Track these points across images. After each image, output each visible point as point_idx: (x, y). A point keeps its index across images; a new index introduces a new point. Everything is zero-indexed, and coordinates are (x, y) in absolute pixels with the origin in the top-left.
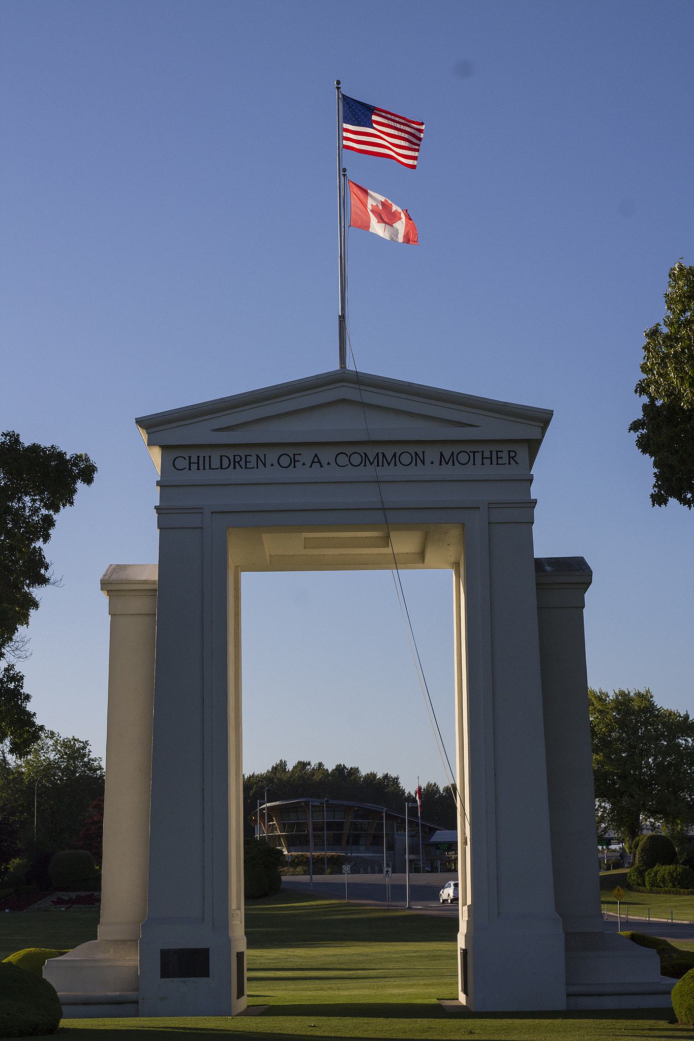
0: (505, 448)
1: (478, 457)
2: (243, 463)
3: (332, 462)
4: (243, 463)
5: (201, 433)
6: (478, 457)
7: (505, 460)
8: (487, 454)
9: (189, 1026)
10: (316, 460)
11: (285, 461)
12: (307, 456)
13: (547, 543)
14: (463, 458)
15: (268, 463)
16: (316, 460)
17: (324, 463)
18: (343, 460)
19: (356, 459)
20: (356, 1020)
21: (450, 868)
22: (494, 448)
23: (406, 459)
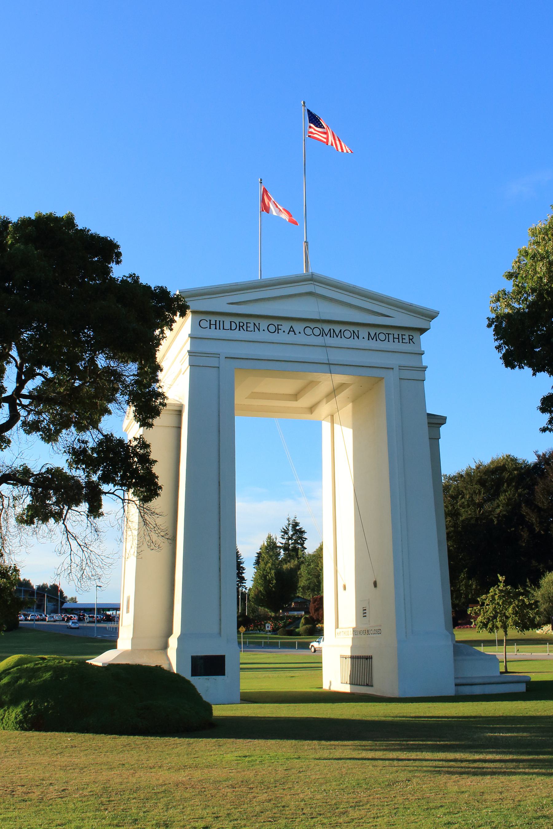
0: (407, 333)
1: (391, 337)
2: (245, 327)
3: (302, 332)
4: (245, 327)
6: (391, 337)
7: (407, 340)
8: (396, 336)
10: (292, 330)
12: (285, 326)
14: (382, 337)
15: (261, 330)
16: (292, 330)
17: (297, 332)
19: (317, 332)
23: (347, 334)
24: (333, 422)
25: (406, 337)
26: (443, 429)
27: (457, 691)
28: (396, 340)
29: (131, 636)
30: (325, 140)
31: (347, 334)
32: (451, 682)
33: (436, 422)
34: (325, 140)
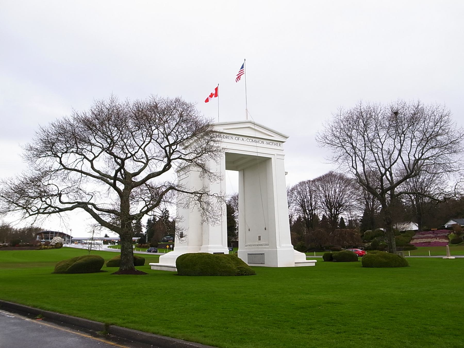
0: (279, 143)
10: (243, 140)
11: (237, 139)
14: (271, 144)
19: (251, 141)
31: (260, 142)
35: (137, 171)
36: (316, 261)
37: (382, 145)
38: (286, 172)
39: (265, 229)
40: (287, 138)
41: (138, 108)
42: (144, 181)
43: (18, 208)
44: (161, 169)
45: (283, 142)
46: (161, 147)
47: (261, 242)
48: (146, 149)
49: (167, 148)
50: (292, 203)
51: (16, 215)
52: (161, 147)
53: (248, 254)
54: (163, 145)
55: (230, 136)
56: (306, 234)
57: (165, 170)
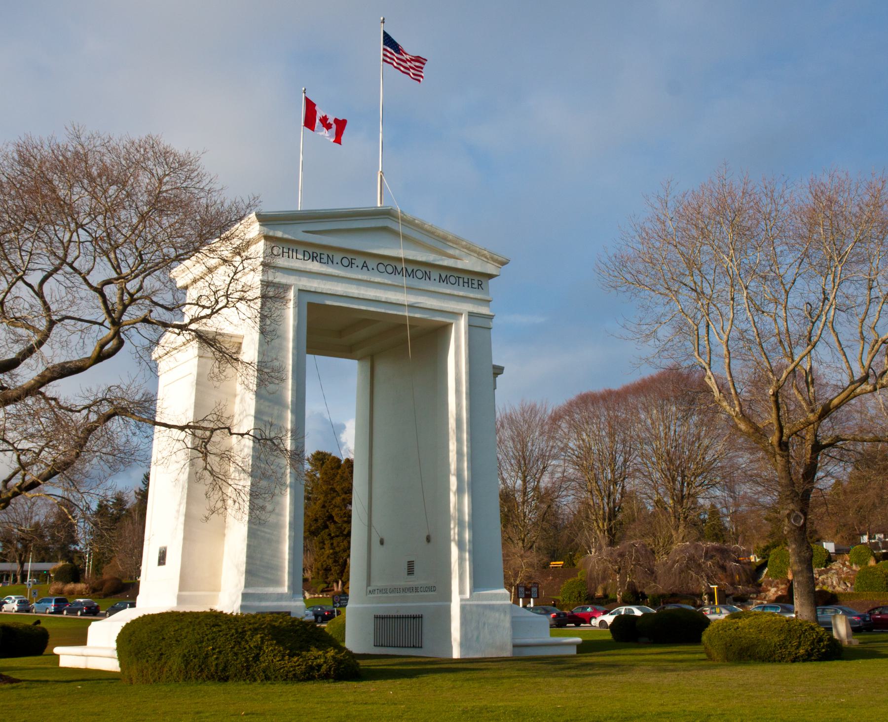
0: (476, 278)
1: (461, 280)
2: (318, 258)
3: (375, 268)
4: (318, 258)
5: (296, 233)
6: (461, 280)
7: (476, 286)
8: (466, 280)
9: (590, 678)
10: (365, 265)
11: (345, 262)
12: (359, 261)
13: (496, 362)
14: (453, 280)
15: (335, 262)
16: (365, 265)
17: (370, 268)
18: (381, 268)
19: (390, 269)
20: (440, 263)
21: (463, 608)
22: (470, 277)
23: (419, 274)
24: (184, 305)
25: (476, 282)
26: (499, 378)
27: (514, 652)
28: (466, 285)
29: (138, 598)
30: (704, 656)
31: (419, 274)
32: (510, 647)
33: (498, 371)
34: (704, 656)
35: (12, 356)
36: (579, 640)
37: (787, 293)
38: (495, 367)
39: (428, 539)
40: (503, 264)
41: (25, 160)
42: (33, 390)
43: (16, 481)
44: (90, 351)
45: (490, 276)
46: (90, 286)
47: (412, 581)
48: (46, 287)
49: (111, 291)
50: (555, 457)
51: (190, 349)
52: (90, 286)
53: (376, 617)
54: (96, 279)
55: (326, 252)
56: (542, 550)
57: (101, 356)
